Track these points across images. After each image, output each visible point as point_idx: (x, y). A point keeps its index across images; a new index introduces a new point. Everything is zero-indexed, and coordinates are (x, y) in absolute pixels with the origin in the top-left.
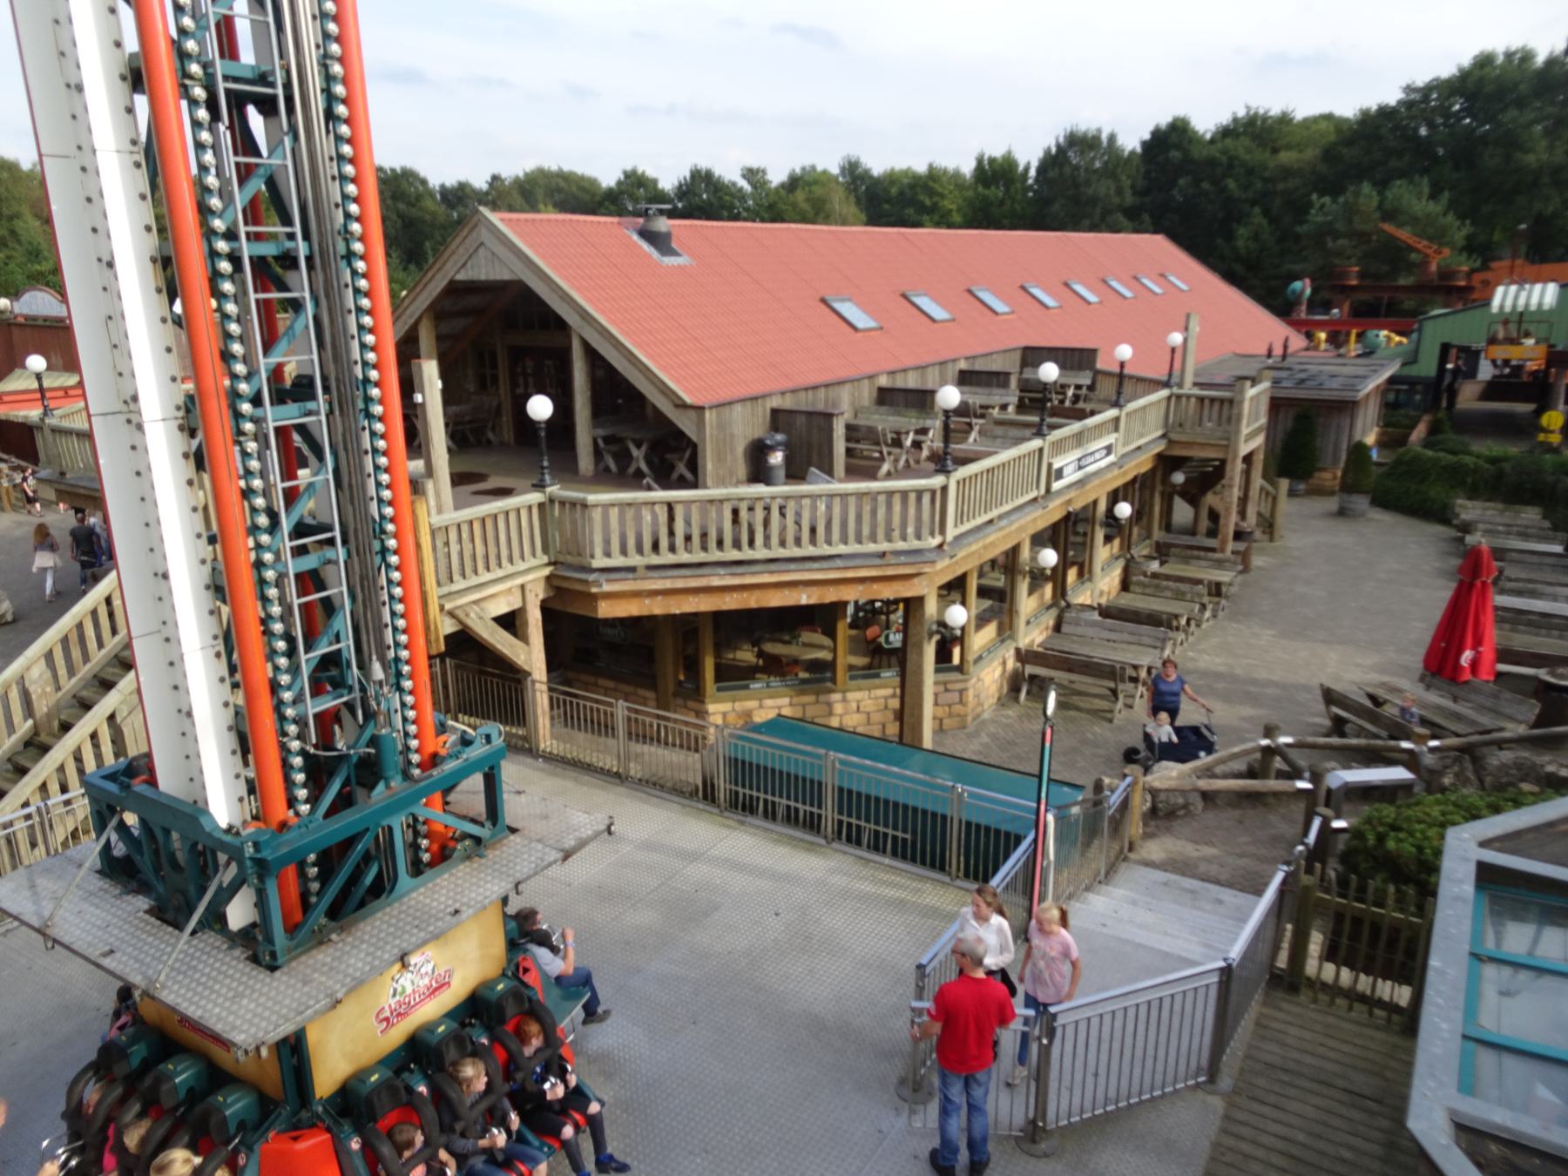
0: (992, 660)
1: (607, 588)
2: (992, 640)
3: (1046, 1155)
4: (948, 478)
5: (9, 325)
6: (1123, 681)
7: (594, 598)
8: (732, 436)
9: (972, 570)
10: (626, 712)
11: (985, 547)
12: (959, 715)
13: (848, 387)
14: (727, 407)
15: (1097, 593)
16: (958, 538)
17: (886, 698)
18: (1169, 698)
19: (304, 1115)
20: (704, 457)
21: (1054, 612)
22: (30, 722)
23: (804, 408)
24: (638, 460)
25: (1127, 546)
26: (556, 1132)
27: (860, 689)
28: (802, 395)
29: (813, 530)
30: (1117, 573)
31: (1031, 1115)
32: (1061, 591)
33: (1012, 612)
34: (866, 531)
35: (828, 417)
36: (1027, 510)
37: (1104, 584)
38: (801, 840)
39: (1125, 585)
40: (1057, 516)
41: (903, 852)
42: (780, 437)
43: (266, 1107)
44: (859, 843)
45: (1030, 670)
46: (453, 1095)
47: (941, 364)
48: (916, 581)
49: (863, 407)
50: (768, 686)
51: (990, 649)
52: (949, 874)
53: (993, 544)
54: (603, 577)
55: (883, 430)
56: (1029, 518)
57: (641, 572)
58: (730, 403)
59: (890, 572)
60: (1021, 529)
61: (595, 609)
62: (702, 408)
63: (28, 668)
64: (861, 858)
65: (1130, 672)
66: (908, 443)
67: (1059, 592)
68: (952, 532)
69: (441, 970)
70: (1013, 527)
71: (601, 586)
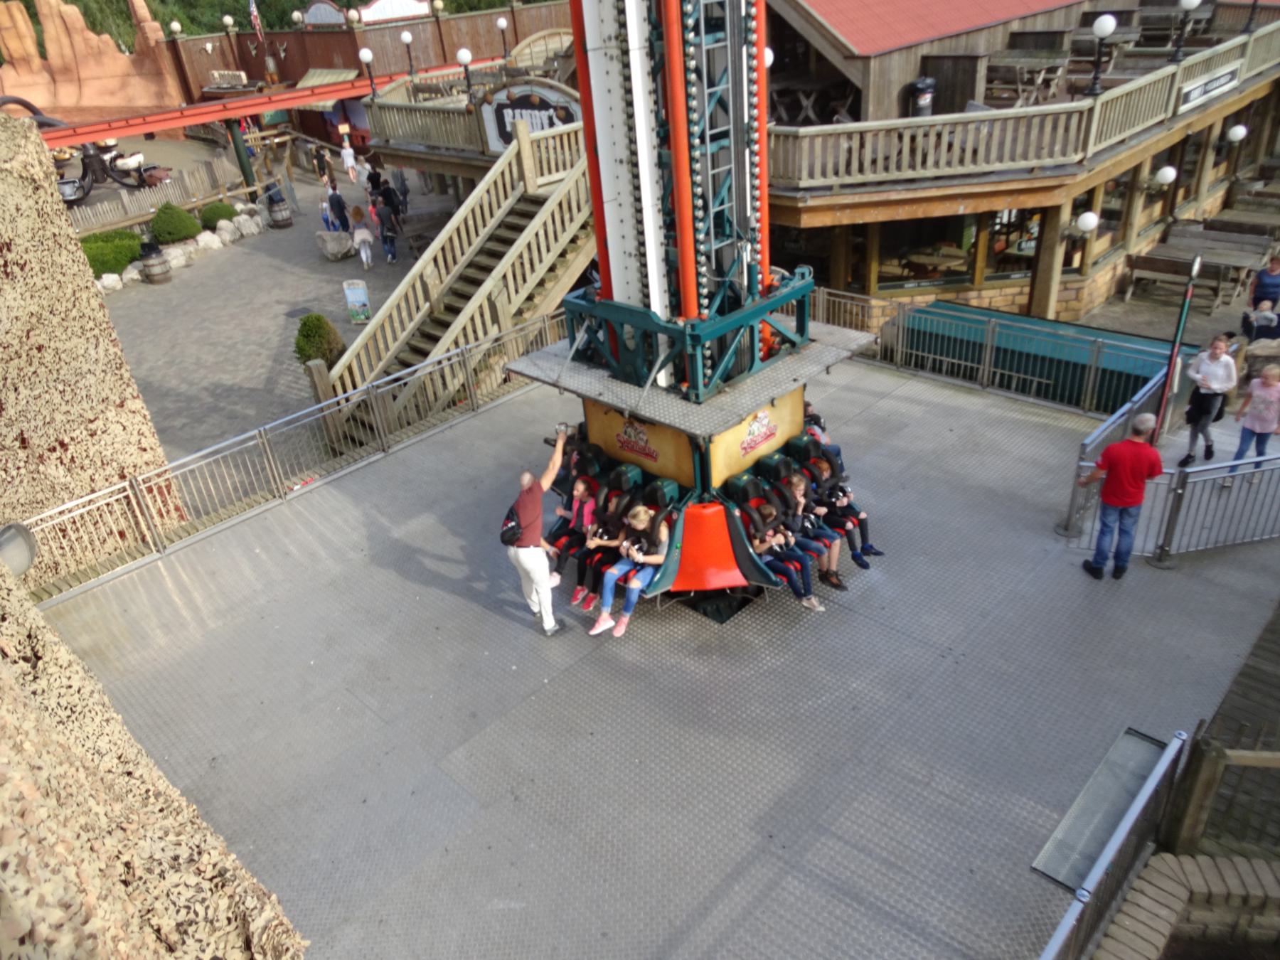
0: (1106, 265)
1: (811, 203)
2: (1105, 250)
3: (1169, 568)
4: (1095, 100)
5: (302, 33)
6: (1225, 279)
7: (798, 211)
8: (890, 82)
9: (1100, 185)
10: (826, 297)
11: (1114, 165)
12: (1074, 310)
13: (985, 33)
14: (887, 56)
15: (1200, 211)
16: (1096, 154)
17: (1014, 295)
18: (1272, 290)
19: (706, 496)
20: (867, 102)
21: (1161, 227)
22: (428, 305)
23: (947, 53)
24: (807, 109)
25: (1232, 170)
26: (842, 526)
27: (994, 288)
28: (947, 42)
29: (975, 152)
30: (1220, 193)
31: (1160, 542)
32: (1169, 208)
33: (1127, 225)
34: (1019, 150)
35: (974, 59)
36: (1154, 131)
37: (1209, 202)
38: (962, 387)
39: (1227, 204)
40: (1177, 138)
41: (1044, 393)
42: (929, 81)
43: (684, 492)
44: (1009, 388)
45: (1138, 273)
46: (788, 494)
47: (1068, 7)
48: (1057, 192)
49: (996, 52)
50: (919, 286)
51: (1105, 255)
52: (1083, 408)
53: (1120, 162)
54: (808, 195)
55: (1021, 68)
56: (1155, 139)
57: (836, 190)
58: (890, 52)
59: (1037, 184)
60: (1145, 150)
61: (799, 221)
62: (866, 59)
63: (425, 268)
64: (1010, 398)
65: (1232, 274)
66: (1039, 80)
67: (1168, 208)
68: (1092, 149)
69: (772, 425)
70: (1141, 147)
71: (806, 201)
